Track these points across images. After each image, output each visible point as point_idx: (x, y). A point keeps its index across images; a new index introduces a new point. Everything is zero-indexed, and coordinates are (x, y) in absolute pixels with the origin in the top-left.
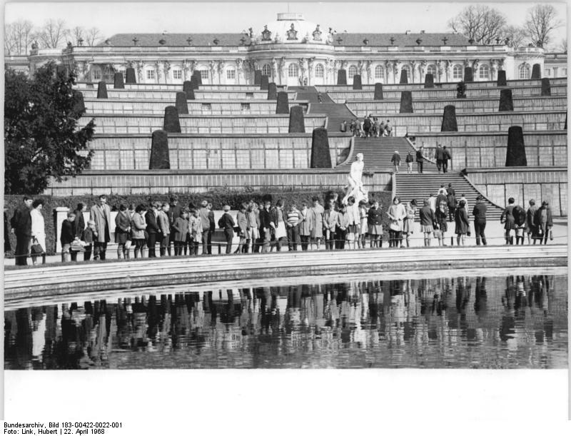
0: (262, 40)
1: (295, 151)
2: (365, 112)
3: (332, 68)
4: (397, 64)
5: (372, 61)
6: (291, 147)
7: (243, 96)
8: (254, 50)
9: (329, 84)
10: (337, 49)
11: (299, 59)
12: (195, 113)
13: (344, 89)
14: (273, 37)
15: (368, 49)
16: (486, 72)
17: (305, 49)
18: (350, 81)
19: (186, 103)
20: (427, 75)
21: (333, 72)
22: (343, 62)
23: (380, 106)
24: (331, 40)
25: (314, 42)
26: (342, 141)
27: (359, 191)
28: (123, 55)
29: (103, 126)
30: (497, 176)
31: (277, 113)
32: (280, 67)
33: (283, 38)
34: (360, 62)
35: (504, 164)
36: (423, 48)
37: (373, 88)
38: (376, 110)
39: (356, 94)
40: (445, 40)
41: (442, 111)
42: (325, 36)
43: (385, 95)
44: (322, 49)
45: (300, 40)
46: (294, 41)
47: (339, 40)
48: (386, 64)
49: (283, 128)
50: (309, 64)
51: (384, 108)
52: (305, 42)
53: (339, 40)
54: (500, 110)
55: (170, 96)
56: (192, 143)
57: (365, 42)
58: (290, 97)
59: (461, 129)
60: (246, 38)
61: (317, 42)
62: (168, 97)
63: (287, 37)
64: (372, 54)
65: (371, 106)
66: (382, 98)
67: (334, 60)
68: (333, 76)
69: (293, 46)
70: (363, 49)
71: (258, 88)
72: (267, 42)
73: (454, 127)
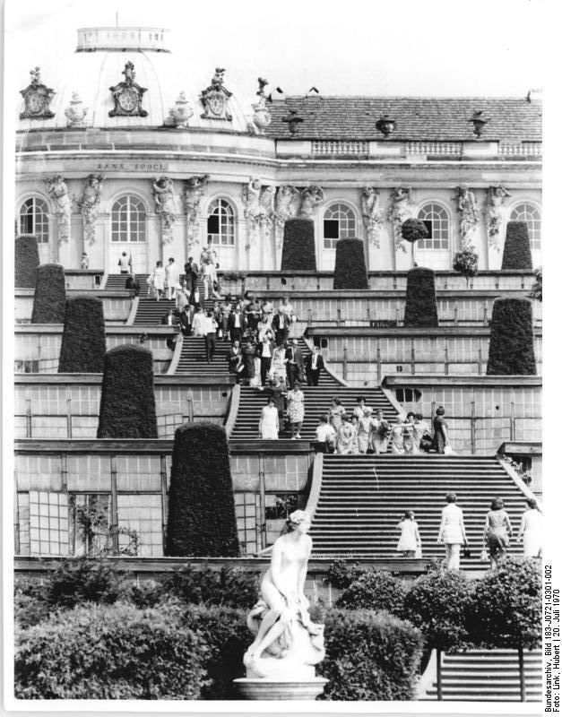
0: (111, 115)
2: (373, 367)
3: (264, 211)
4: (497, 201)
5: (406, 191)
9: (254, 268)
10: (284, 148)
11: (151, 181)
13: (308, 285)
14: (58, 106)
15: (395, 150)
16: (133, 226)
17: (171, 147)
18: (326, 258)
19: (103, 325)
21: (266, 229)
22: (303, 193)
23: (423, 349)
24: (264, 118)
25: (205, 124)
26: (283, 466)
27: (295, 627)
32: (81, 205)
33: (97, 113)
34: (364, 193)
37: (402, 284)
38: (413, 363)
40: (478, 123)
42: (243, 107)
43: (444, 311)
44: (232, 150)
45: (156, 119)
47: (293, 121)
48: (457, 200)
49: (82, 421)
50: (184, 197)
51: (441, 355)
52: (171, 126)
53: (291, 119)
54: (61, 369)
56: (64, 473)
57: (381, 125)
58: (110, 310)
63: (111, 108)
65: (392, 349)
66: (434, 322)
67: (273, 184)
68: (268, 239)
69: (130, 138)
70: (374, 149)
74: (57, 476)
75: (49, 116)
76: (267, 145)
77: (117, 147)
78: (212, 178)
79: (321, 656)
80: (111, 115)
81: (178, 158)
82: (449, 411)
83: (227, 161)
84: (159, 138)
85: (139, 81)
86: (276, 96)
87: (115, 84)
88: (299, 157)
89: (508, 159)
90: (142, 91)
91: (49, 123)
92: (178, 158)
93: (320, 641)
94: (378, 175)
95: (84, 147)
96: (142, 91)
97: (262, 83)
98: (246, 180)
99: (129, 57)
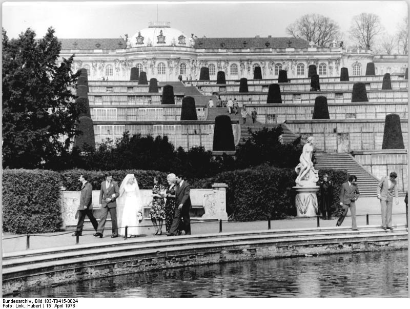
0: (158, 43)
1: (189, 136)
6: (186, 133)
7: (125, 90)
8: (129, 52)
12: (287, 103)
15: (225, 51)
19: (87, 95)
20: (342, 69)
23: (246, 98)
25: (179, 45)
26: (366, 126)
28: (124, 56)
29: (336, 114)
30: (380, 157)
31: (268, 103)
35: (381, 147)
36: (271, 50)
39: (143, 88)
40: (76, 44)
41: (313, 102)
42: (189, 41)
46: (162, 44)
55: (298, 88)
59: (332, 117)
60: (122, 43)
61: (182, 45)
62: (296, 89)
63: (157, 41)
64: (228, 55)
69: (162, 48)
71: (136, 84)
72: (140, 45)
73: (326, 115)
74: (186, 130)
75: (143, 43)
76: (194, 50)
77: (159, 51)
78: (182, 58)
79: (317, 180)
80: (158, 43)
81: (173, 53)
82: (258, 113)
83: (185, 54)
84: (168, 48)
85: (164, 35)
86: (195, 38)
87: (158, 35)
88: (202, 53)
89: (252, 52)
90: (164, 37)
91: (143, 45)
92: (173, 53)
93: (317, 175)
94: (221, 57)
95: (151, 51)
96: (164, 37)
97: (192, 35)
98: (189, 58)
99: (161, 29)
